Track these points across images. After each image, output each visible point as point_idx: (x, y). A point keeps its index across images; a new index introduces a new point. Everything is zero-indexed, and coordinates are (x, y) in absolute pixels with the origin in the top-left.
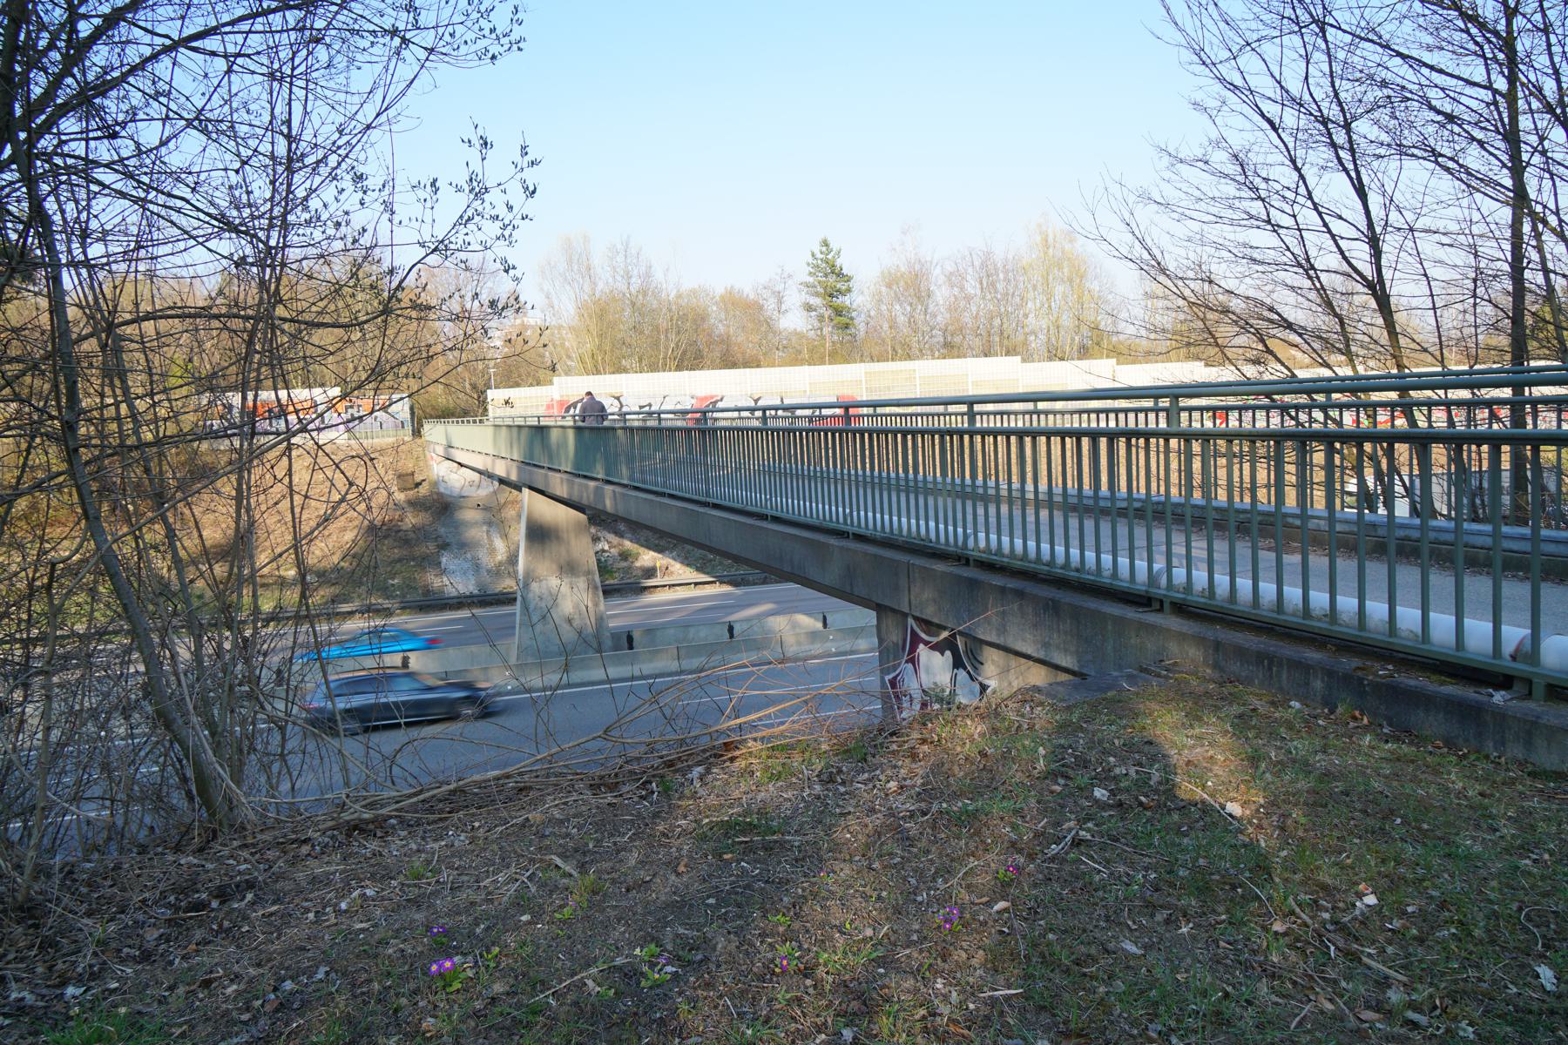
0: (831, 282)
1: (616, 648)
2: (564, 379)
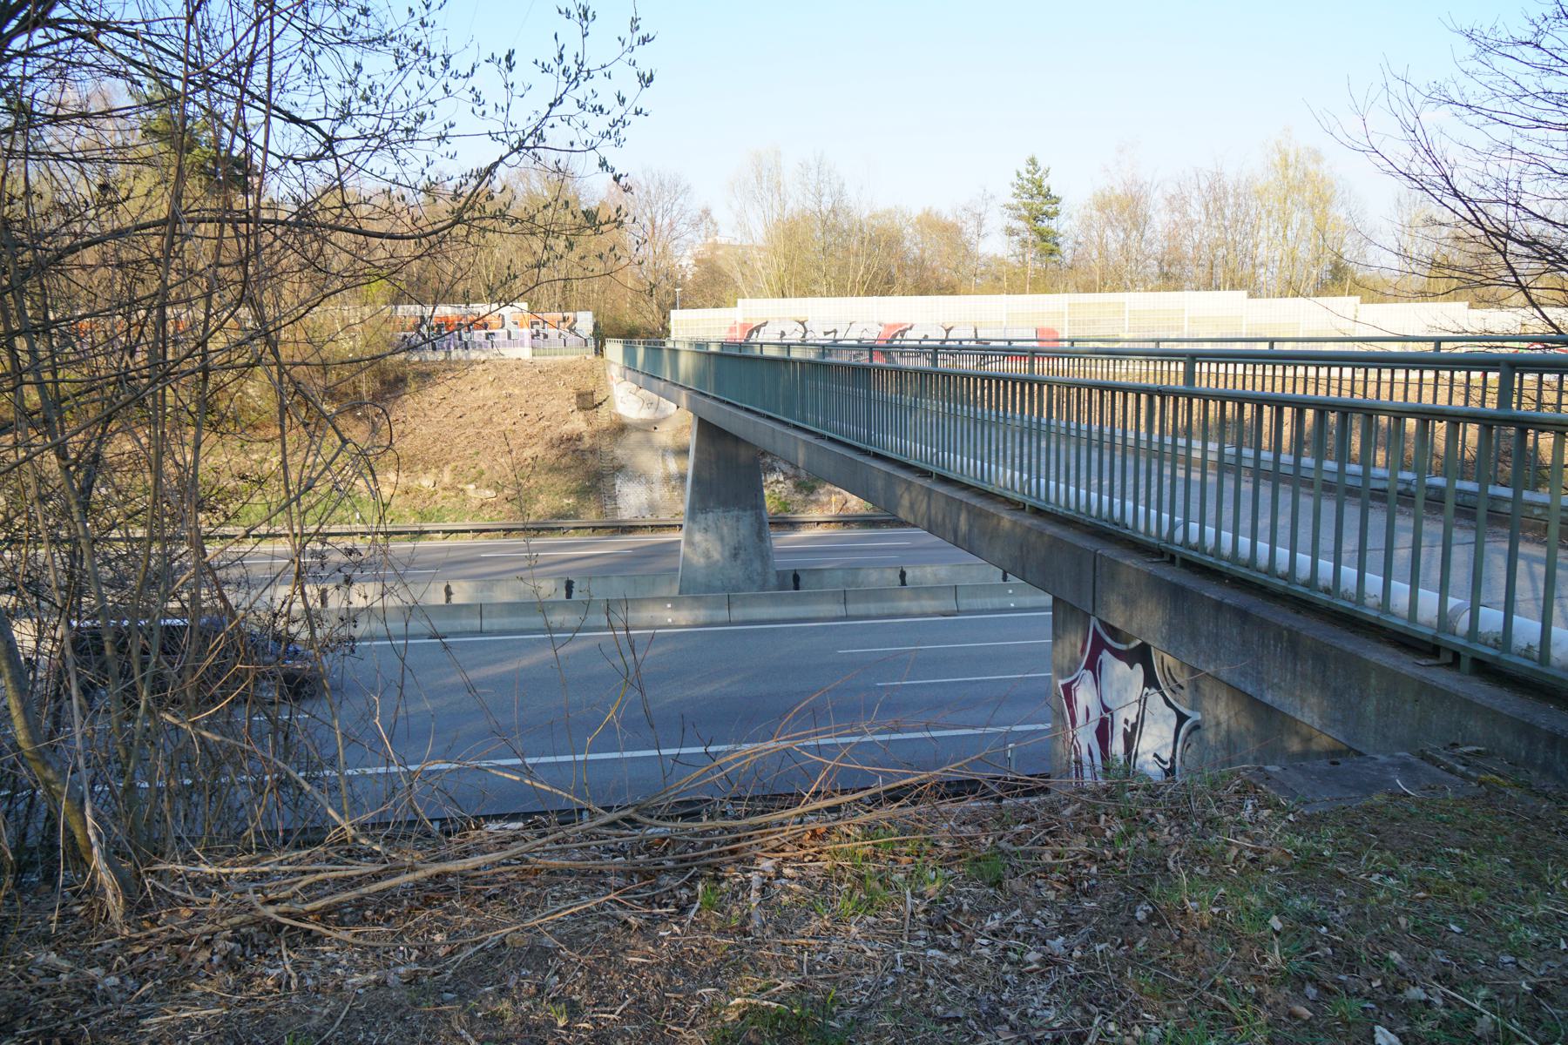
0: (1037, 204)
1: (782, 587)
2: (748, 300)
